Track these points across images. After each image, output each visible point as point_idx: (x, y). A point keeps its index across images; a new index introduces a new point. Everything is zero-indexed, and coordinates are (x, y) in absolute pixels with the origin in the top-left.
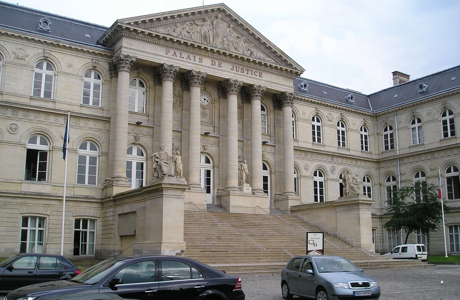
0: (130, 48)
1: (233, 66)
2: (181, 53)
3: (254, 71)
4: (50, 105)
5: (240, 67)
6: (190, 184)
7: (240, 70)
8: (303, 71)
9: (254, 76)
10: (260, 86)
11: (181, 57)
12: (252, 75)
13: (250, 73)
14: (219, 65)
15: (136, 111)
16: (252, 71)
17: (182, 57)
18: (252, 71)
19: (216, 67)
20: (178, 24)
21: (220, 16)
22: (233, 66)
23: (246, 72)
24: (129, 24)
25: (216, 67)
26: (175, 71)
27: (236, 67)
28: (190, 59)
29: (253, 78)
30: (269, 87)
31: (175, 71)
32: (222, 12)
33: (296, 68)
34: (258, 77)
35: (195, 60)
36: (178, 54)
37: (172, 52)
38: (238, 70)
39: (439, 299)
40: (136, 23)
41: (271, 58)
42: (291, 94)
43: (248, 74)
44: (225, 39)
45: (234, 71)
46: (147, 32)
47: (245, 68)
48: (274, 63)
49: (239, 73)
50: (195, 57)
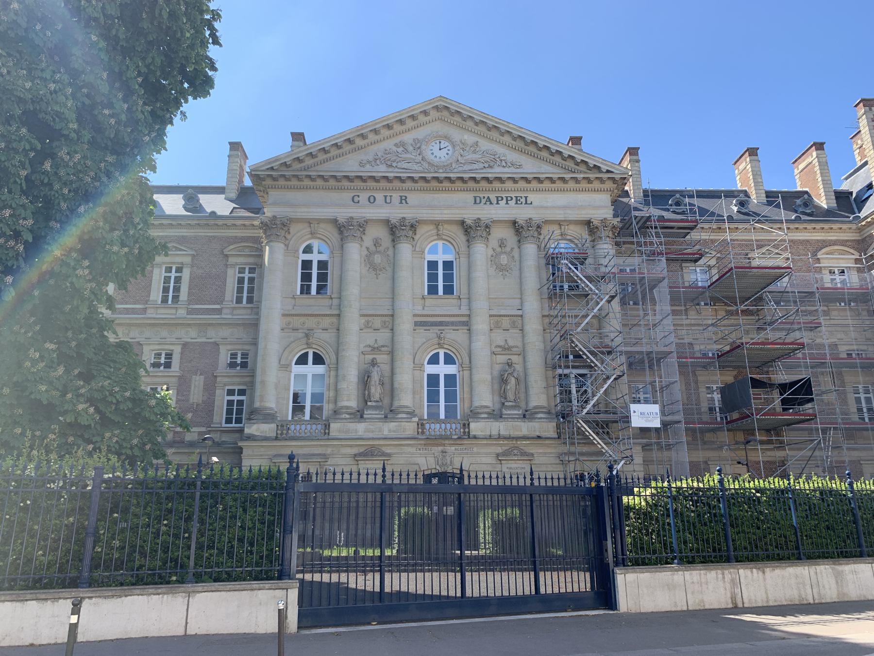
11: (526, 203)
24: (272, 168)
28: (491, 203)
32: (444, 110)
33: (608, 171)
40: (285, 164)
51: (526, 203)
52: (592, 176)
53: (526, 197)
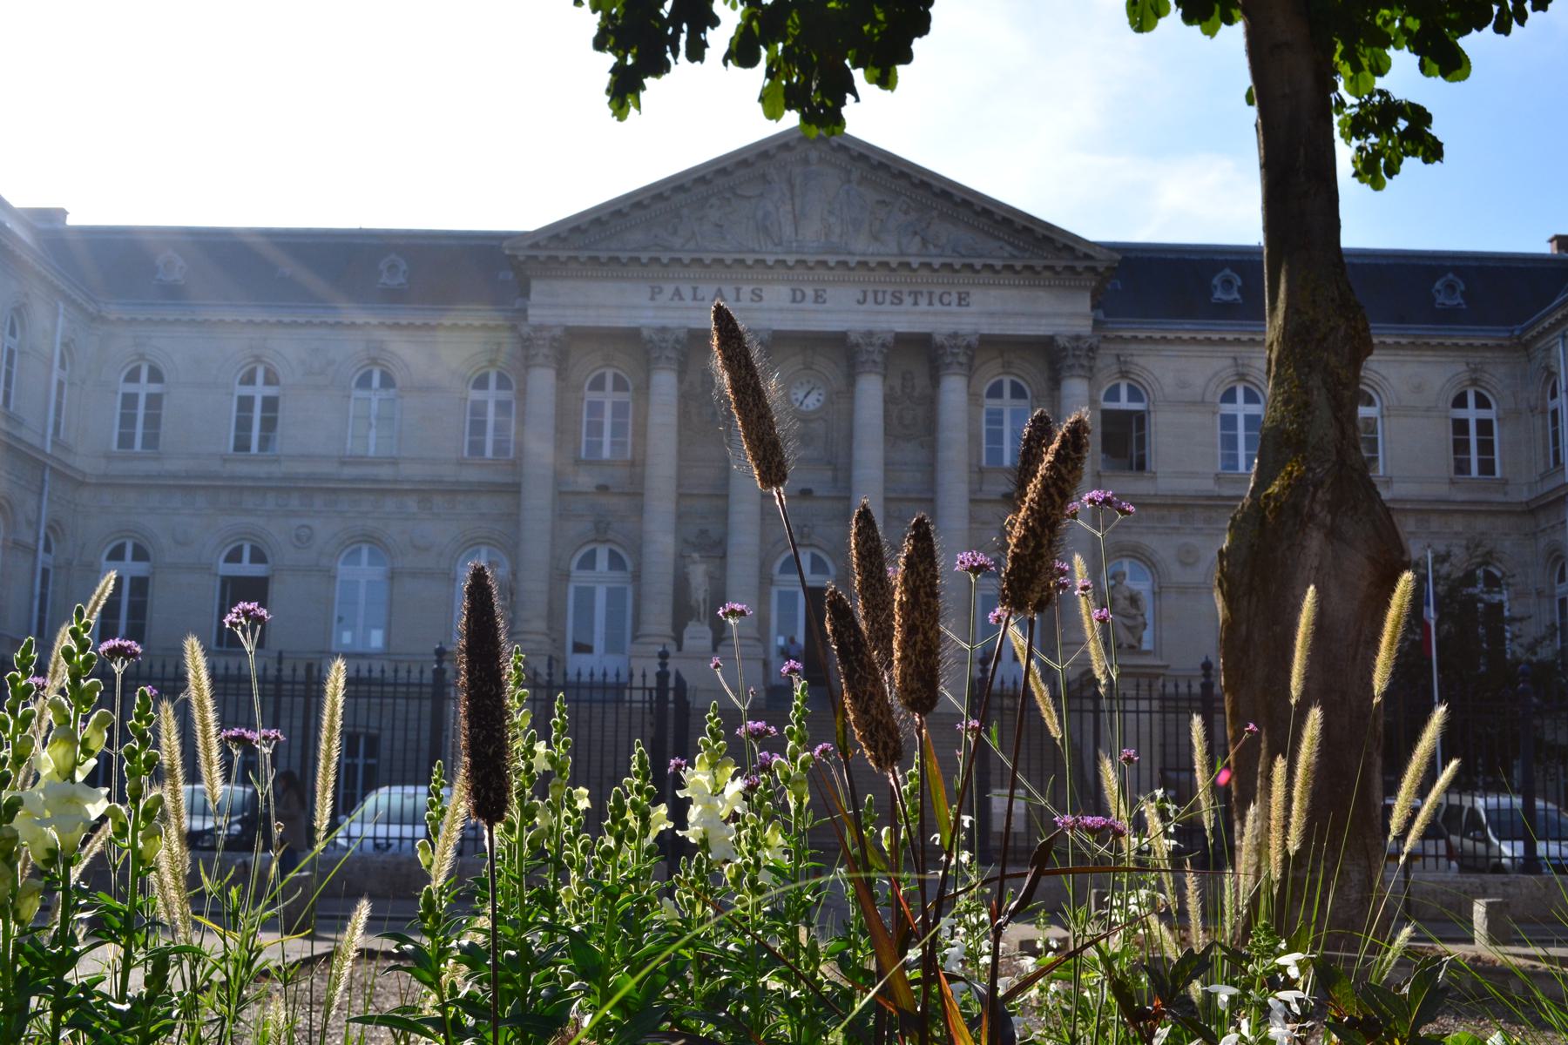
0: (562, 304)
1: (865, 293)
2: (695, 289)
3: (938, 291)
4: (262, 470)
5: (890, 289)
6: (1207, 686)
7: (888, 298)
8: (63, 213)
9: (937, 306)
10: (955, 335)
12: (931, 304)
13: (923, 305)
14: (960, 299)
15: (372, 452)
16: (931, 294)
17: (700, 295)
18: (931, 294)
19: (809, 304)
20: (685, 211)
21: (814, 155)
22: (865, 293)
23: (908, 300)
25: (809, 304)
26: (677, 341)
27: (876, 293)
29: (935, 314)
30: (985, 330)
31: (883, 345)
34: (954, 308)
35: (738, 299)
36: (686, 290)
37: (669, 289)
38: (880, 298)
39: (836, 1036)
41: (999, 239)
42: (1078, 338)
43: (916, 303)
44: (832, 220)
45: (870, 305)
46: (604, 256)
47: (906, 290)
48: (1014, 257)
49: (887, 307)
50: (738, 290)
51: (695, 298)
52: (1060, 264)
53: (695, 289)
